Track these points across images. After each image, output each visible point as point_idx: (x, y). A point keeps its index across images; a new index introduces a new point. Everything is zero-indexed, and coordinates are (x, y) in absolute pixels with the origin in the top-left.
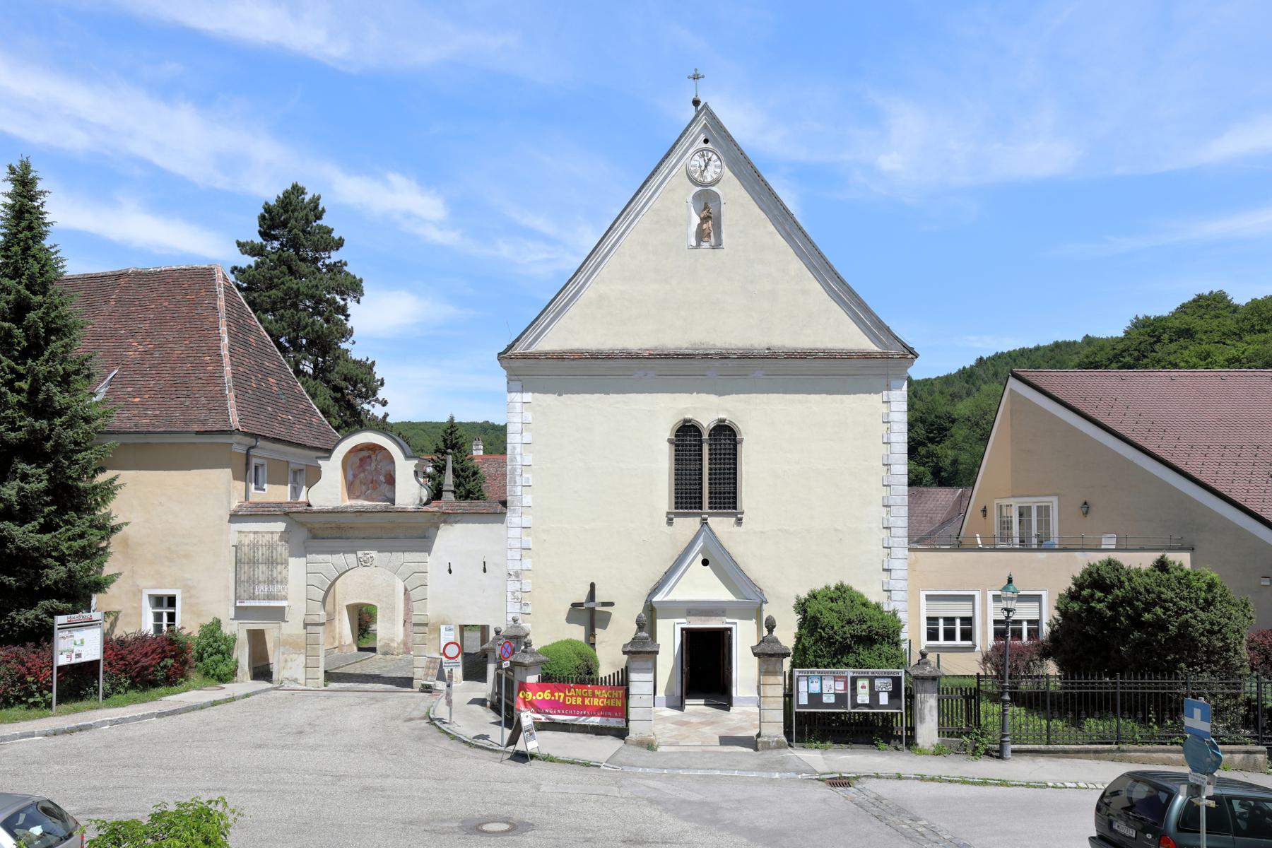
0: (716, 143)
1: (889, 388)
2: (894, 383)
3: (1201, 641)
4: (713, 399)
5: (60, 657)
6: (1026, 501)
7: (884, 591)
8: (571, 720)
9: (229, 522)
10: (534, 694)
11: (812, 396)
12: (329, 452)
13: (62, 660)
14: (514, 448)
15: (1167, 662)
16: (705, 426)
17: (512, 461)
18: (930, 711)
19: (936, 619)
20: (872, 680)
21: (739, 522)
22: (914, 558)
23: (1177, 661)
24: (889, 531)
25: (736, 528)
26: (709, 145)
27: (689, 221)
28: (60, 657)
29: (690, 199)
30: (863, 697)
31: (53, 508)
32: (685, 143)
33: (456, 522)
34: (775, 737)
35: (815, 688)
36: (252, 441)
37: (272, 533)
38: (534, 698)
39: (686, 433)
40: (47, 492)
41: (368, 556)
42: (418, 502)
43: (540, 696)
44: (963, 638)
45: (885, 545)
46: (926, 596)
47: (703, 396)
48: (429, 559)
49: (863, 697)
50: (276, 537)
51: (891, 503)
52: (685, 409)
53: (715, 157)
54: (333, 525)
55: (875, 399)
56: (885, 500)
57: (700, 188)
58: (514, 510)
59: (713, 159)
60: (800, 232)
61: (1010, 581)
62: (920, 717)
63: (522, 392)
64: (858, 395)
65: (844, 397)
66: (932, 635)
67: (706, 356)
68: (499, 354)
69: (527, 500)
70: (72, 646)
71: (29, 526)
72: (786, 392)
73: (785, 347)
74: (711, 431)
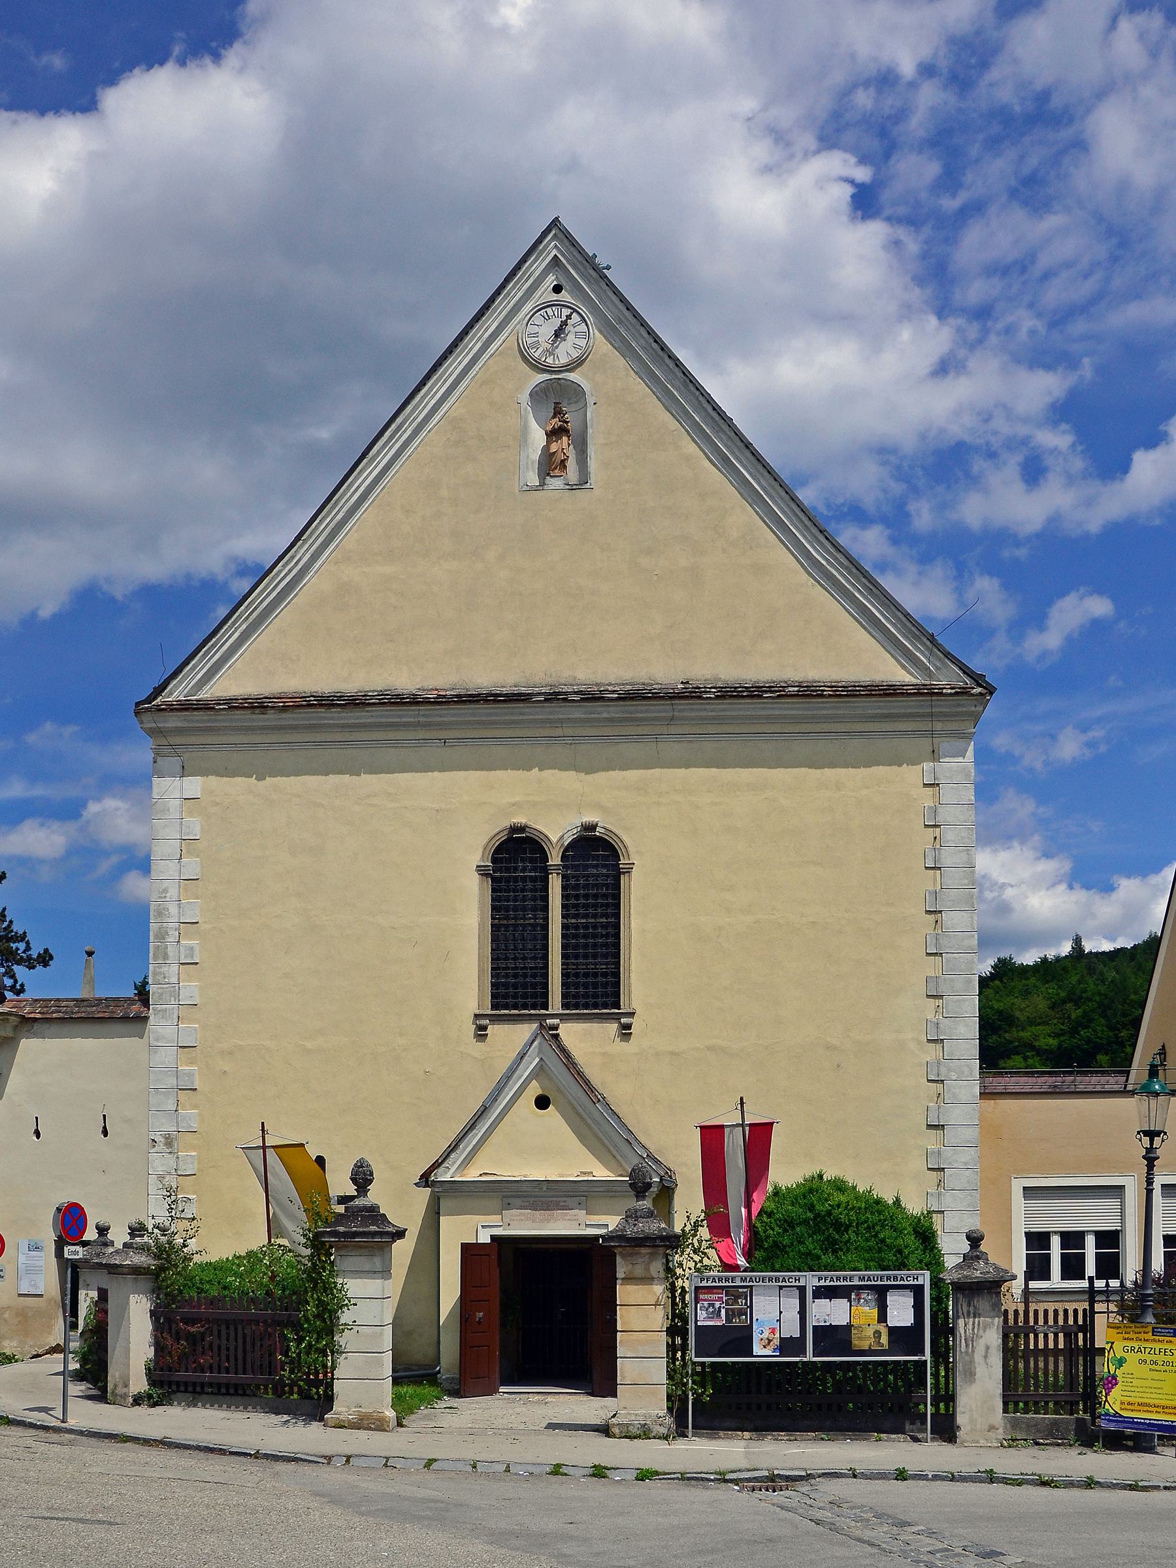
1: (935, 755)
7: (929, 1169)
16: (554, 839)
21: (625, 1031)
25: (620, 1046)
26: (565, 296)
44: (1064, 1277)
55: (911, 776)
56: (932, 985)
57: (546, 376)
67: (554, 697)
68: (138, 704)
74: (566, 850)
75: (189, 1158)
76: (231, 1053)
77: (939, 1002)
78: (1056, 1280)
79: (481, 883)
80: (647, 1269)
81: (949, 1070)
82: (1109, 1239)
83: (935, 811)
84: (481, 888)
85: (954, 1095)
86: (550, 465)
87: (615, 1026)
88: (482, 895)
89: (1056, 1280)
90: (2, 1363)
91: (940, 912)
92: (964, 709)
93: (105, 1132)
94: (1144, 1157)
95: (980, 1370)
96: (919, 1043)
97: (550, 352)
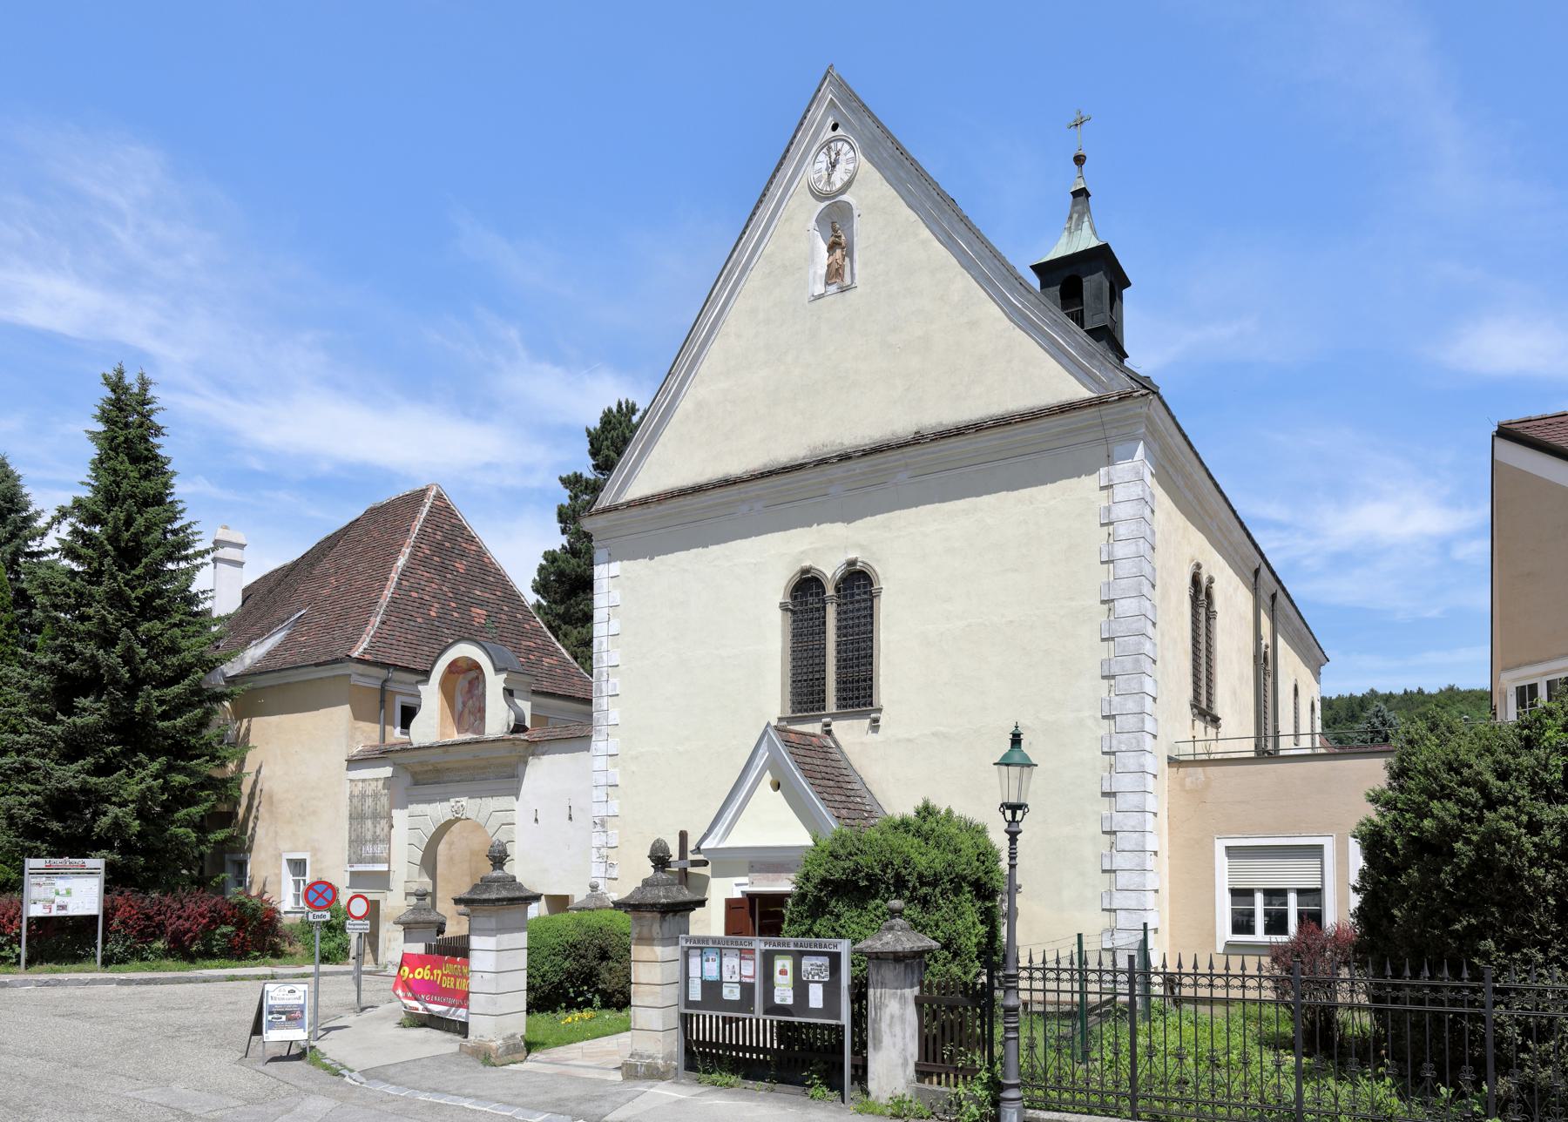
0: (850, 128)
1: (1110, 460)
2: (1118, 450)
3: (1532, 880)
4: (838, 529)
5: (32, 907)
6: (1526, 676)
7: (1104, 832)
8: (439, 1012)
9: (347, 769)
10: (412, 971)
11: (985, 498)
12: (426, 674)
13: (36, 911)
14: (601, 643)
15: (1455, 935)
16: (829, 576)
17: (598, 662)
18: (891, 1025)
19: (1249, 893)
20: (798, 956)
21: (875, 725)
22: (1202, 777)
23: (1477, 933)
24: (1112, 722)
25: (872, 736)
26: (840, 131)
27: (811, 258)
28: (32, 907)
29: (812, 223)
30: (784, 993)
31: (117, 748)
32: (804, 139)
33: (544, 754)
34: (649, 1057)
35: (711, 972)
36: (383, 673)
37: (377, 780)
38: (411, 976)
39: (806, 587)
40: (108, 729)
41: (459, 804)
42: (506, 730)
43: (419, 973)
44: (1269, 930)
45: (1106, 750)
46: (1228, 848)
47: (826, 527)
48: (516, 805)
49: (784, 993)
50: (380, 784)
51: (1115, 670)
52: (802, 553)
53: (846, 147)
54: (431, 767)
55: (1087, 486)
56: (1106, 667)
57: (827, 203)
58: (600, 731)
59: (844, 151)
60: (963, 225)
61: (1016, 740)
62: (874, 1038)
63: (609, 562)
64: (1058, 483)
65: (1033, 490)
66: (1243, 924)
67: (822, 462)
69: (614, 716)
70: (52, 896)
71: (75, 767)
72: (944, 499)
73: (941, 424)
75: (614, 838)
76: (637, 758)
77: (1112, 682)
78: (1260, 936)
79: (783, 616)
80: (650, 931)
81: (1120, 743)
82: (1312, 895)
83: (1109, 509)
84: (783, 620)
85: (1124, 766)
86: (834, 274)
87: (869, 720)
88: (783, 626)
89: (1260, 936)
90: (2, 987)
91: (1113, 600)
92: (1132, 413)
93: (570, 818)
94: (1006, 831)
95: (886, 1040)
96: (1096, 719)
97: (829, 182)
